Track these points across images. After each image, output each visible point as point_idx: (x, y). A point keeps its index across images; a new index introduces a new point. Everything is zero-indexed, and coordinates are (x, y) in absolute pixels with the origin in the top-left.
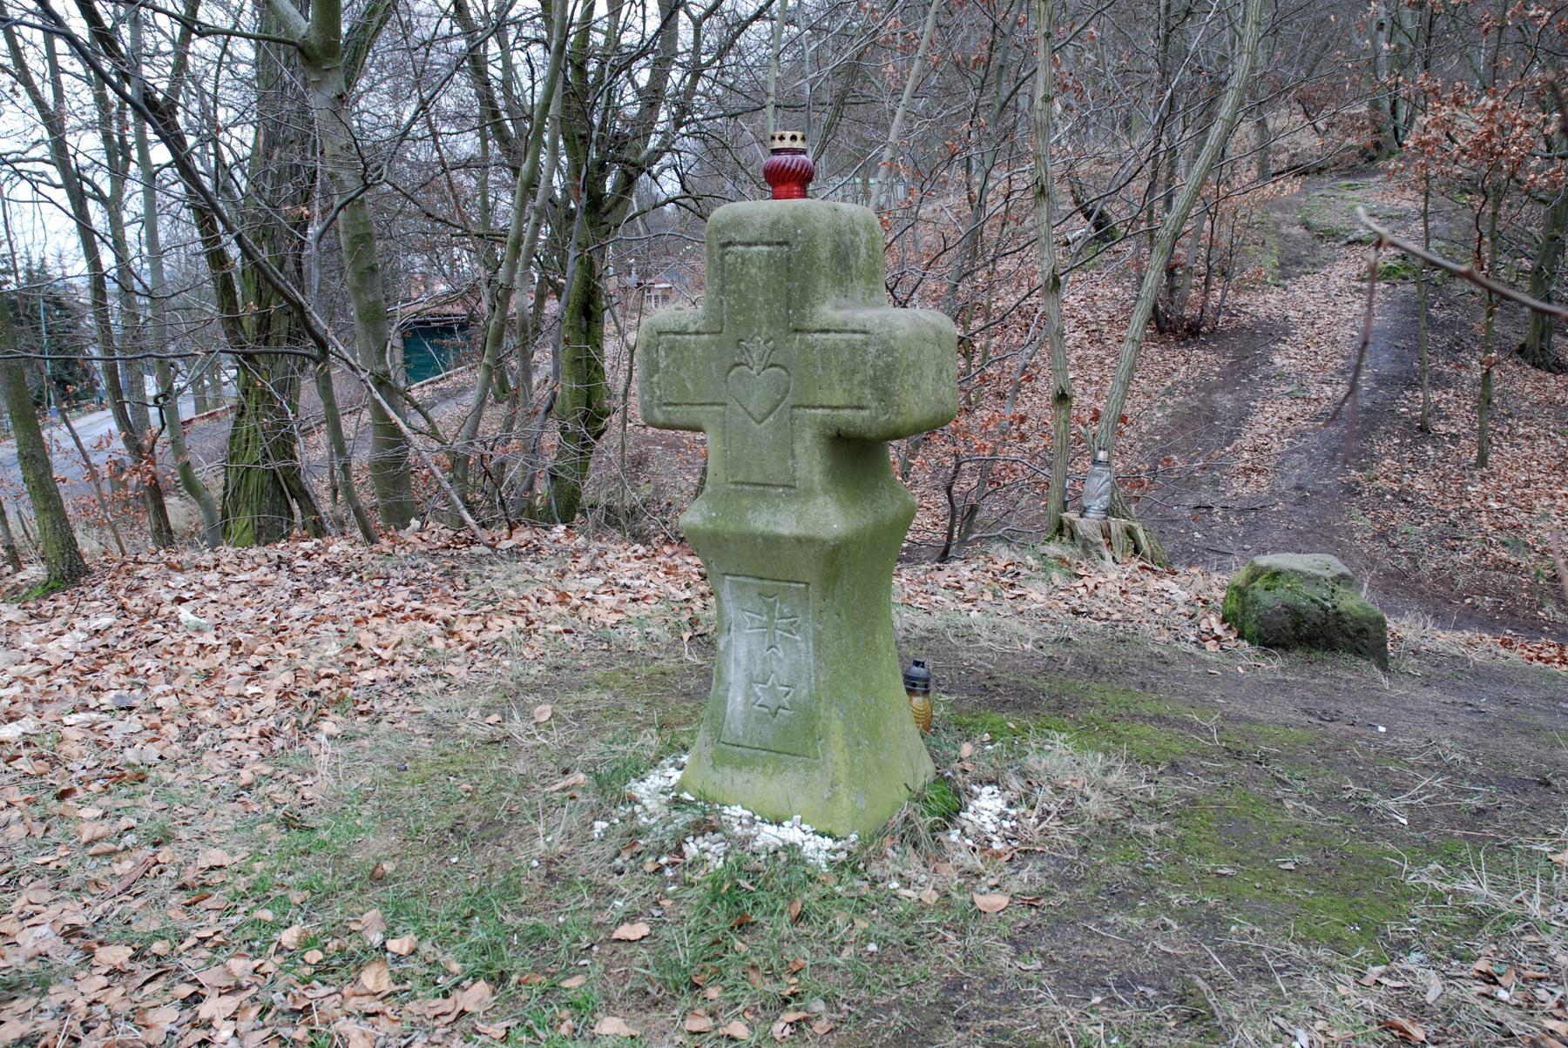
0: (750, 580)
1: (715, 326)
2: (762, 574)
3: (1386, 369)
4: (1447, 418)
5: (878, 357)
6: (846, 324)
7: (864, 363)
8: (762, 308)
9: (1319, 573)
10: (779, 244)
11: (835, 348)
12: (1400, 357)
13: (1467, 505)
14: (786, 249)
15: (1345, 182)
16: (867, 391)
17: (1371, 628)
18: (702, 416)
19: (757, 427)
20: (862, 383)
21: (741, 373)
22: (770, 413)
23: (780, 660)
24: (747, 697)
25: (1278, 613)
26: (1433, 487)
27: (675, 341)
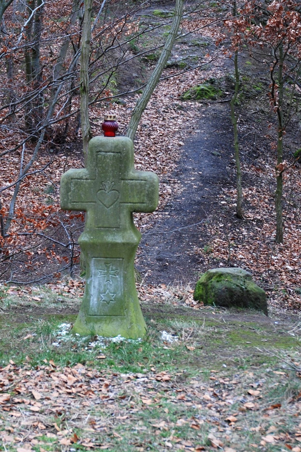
0: (102, 259)
1: (92, 176)
2: (108, 256)
3: (207, 172)
4: (253, 208)
5: (149, 188)
6: (139, 177)
7: (145, 189)
8: (110, 172)
9: (238, 274)
10: (117, 153)
11: (136, 185)
12: (216, 162)
13: (272, 268)
14: (119, 154)
15: (157, 11)
16: (145, 198)
17: (261, 297)
18: (87, 206)
19: (107, 209)
20: (144, 196)
21: (102, 193)
22: (112, 205)
23: (111, 285)
24: (98, 298)
25: (223, 291)
26: (250, 256)
27: (78, 181)
